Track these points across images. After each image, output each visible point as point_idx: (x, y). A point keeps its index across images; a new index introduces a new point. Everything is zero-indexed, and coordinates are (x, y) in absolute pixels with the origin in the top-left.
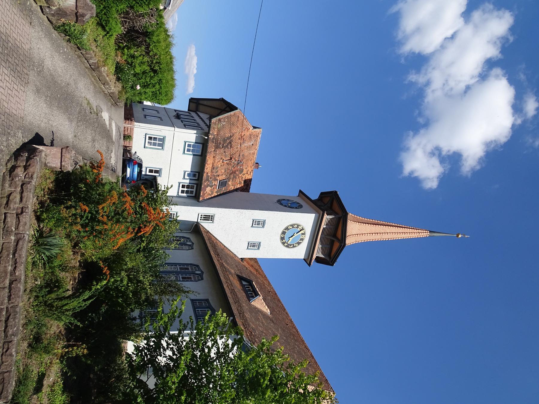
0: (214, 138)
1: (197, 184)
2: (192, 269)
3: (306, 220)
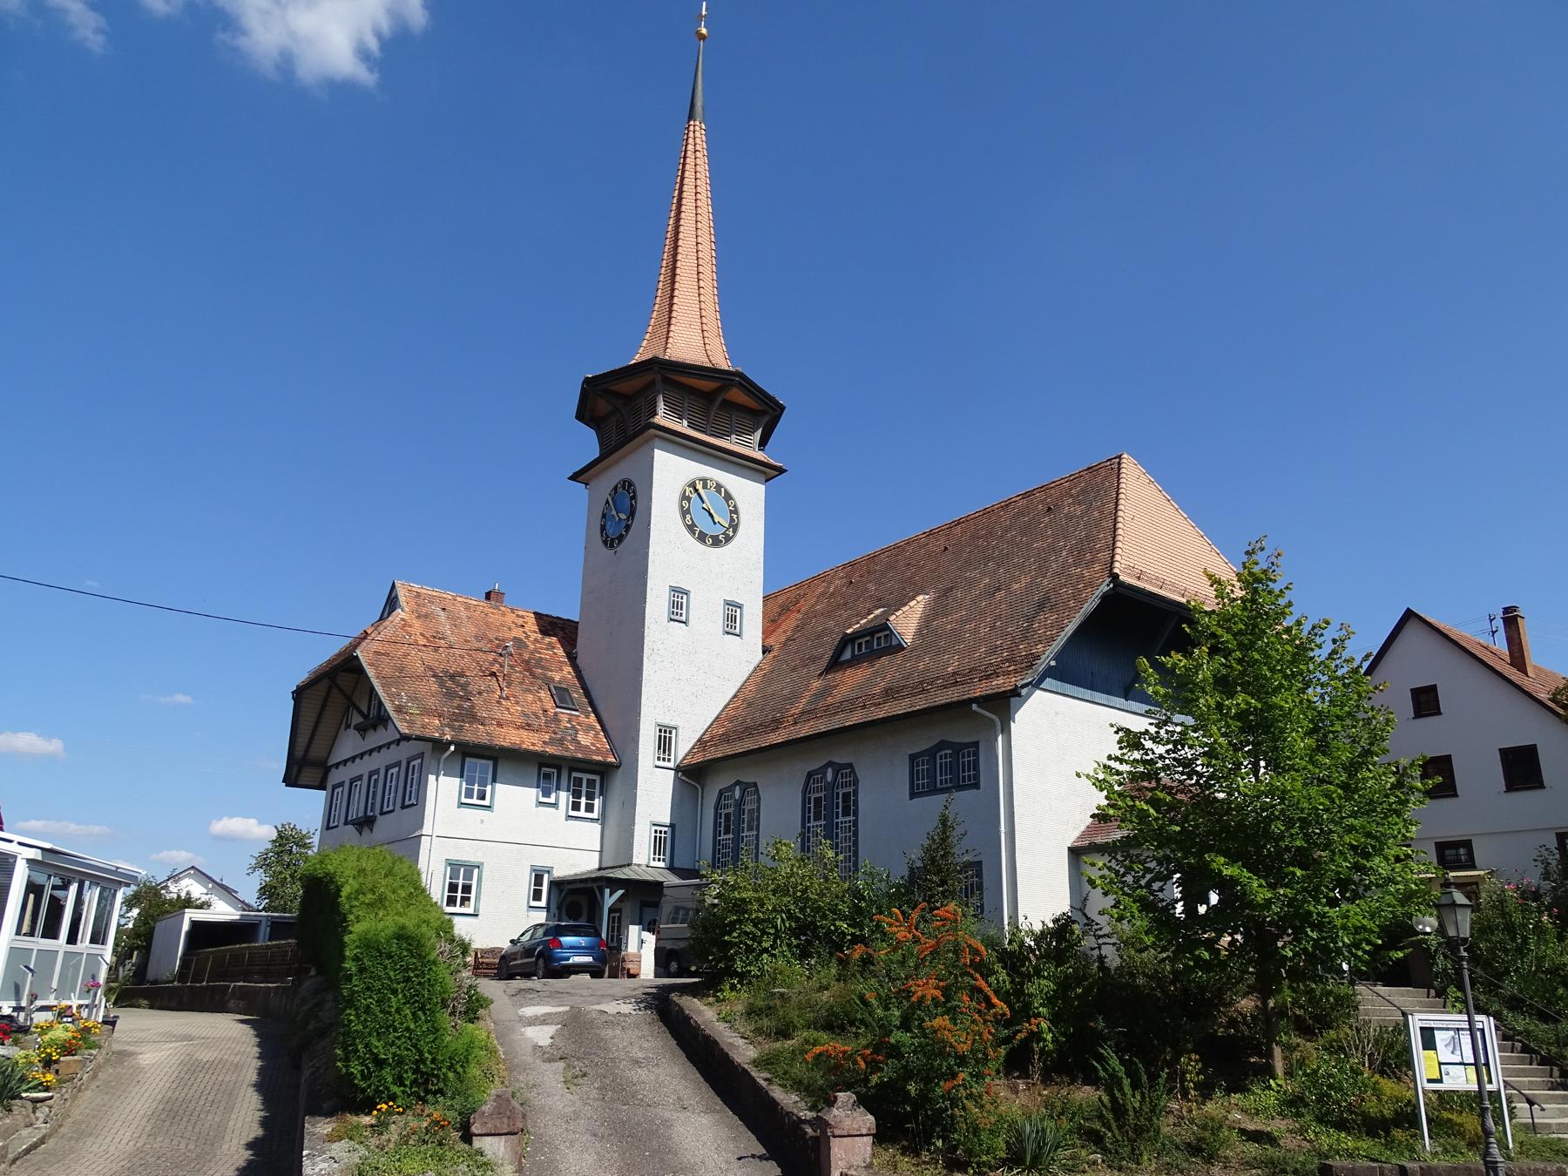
0: (448, 725)
1: (571, 770)
2: (818, 790)
3: (670, 473)
